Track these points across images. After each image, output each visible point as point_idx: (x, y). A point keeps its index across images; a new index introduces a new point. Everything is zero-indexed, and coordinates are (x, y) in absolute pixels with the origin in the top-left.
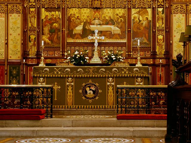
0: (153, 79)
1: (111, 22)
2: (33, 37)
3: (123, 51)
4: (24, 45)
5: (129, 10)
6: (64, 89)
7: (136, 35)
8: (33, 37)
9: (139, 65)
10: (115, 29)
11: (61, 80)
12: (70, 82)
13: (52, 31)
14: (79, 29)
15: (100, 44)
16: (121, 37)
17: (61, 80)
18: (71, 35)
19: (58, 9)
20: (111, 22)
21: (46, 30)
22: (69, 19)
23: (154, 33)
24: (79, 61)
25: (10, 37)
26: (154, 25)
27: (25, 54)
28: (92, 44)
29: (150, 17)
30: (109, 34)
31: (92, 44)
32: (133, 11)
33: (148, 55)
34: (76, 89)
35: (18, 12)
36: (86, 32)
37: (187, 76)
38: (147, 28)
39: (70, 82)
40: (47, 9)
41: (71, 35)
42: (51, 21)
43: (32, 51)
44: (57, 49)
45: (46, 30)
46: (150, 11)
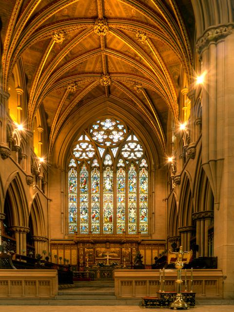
0: (18, 185)
1: (114, 252)
2: (82, 257)
3: (119, 262)
4: (78, 260)
5: (121, 249)
6: (96, 273)
7: (124, 256)
8: (82, 257)
9: (125, 266)
10: (115, 255)
11: (95, 271)
12: (98, 271)
13: (89, 255)
14: (101, 254)
15: (109, 259)
16: (118, 257)
17: (95, 271)
18: (97, 256)
19: (92, 248)
20: (114, 252)
21: (87, 255)
22: (97, 251)
23: (132, 256)
24: (101, 265)
25: (72, 257)
26: (132, 253)
27: (79, 263)
28: (106, 259)
29: (130, 251)
30: (113, 256)
31: (106, 259)
32: (123, 249)
33: (129, 263)
34: (101, 273)
35: (45, 240)
36: (103, 256)
37: (81, 262)
38: (129, 254)
39: (98, 271)
40: (87, 248)
41: (97, 256)
42: (89, 252)
43: (81, 262)
44: (92, 261)
45: (87, 255)
46: (130, 249)
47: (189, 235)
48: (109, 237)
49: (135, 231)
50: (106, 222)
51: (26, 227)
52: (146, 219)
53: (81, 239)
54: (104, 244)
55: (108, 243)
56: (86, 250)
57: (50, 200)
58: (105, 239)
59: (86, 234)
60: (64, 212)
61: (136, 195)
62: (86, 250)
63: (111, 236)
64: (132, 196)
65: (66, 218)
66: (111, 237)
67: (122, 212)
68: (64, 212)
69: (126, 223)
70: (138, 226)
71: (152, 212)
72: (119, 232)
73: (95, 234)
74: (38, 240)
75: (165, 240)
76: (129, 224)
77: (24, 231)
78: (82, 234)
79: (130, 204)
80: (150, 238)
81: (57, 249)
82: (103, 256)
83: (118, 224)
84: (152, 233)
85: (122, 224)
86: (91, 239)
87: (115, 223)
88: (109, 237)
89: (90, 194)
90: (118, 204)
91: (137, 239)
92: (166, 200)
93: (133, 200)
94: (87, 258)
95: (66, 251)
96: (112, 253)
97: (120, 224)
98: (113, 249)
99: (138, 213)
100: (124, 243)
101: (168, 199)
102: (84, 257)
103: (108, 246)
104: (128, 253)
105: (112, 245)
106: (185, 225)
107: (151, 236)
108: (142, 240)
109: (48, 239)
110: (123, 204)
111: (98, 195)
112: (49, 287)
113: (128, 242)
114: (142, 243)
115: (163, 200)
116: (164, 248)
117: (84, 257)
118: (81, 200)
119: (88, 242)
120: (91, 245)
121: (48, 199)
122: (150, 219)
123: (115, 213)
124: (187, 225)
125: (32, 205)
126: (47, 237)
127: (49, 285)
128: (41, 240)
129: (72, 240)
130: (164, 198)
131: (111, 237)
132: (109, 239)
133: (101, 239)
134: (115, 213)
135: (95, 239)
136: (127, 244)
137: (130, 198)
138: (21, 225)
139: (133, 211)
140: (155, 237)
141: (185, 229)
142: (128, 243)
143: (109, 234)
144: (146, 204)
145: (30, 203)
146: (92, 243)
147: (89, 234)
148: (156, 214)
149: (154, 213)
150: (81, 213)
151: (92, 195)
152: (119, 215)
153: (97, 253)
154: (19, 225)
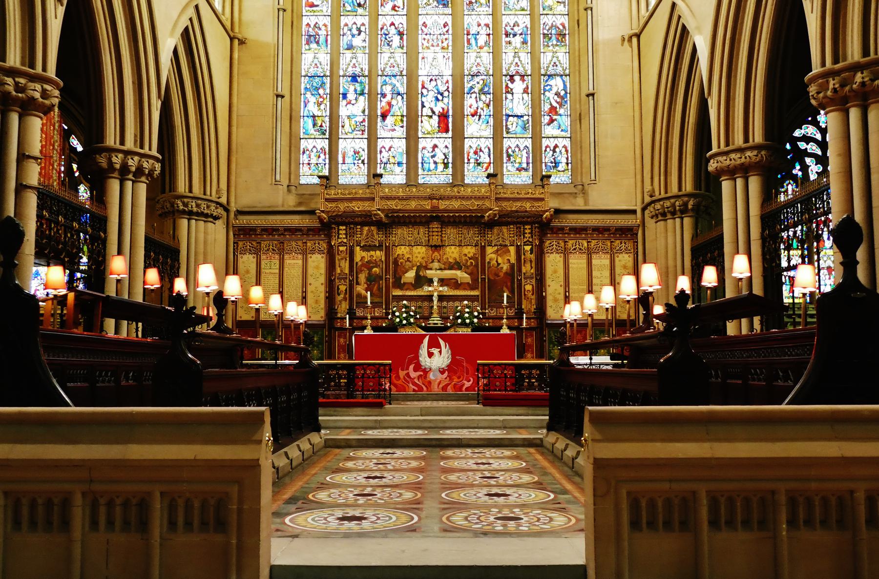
2: (343, 288)
5: (483, 249)
8: (343, 288)
10: (462, 275)
14: (410, 275)
15: (441, 298)
18: (399, 285)
19: (380, 247)
20: (456, 266)
21: (362, 277)
22: (396, 262)
28: (430, 298)
29: (513, 260)
32: (489, 250)
36: (421, 281)
40: (365, 248)
42: (369, 265)
45: (362, 277)
46: (512, 249)
47: (755, 183)
48: (441, 198)
49: (526, 170)
50: (429, 135)
51: (146, 150)
52: (564, 121)
53: (342, 207)
54: (422, 230)
55: (435, 225)
56: (359, 254)
57: (242, 42)
58: (427, 205)
59: (361, 186)
60: (286, 93)
61: (527, 19)
62: (359, 254)
63: (448, 192)
64: (516, 24)
65: (293, 118)
66: (449, 198)
67: (482, 92)
68: (286, 93)
69: (497, 137)
70: (537, 150)
71: (585, 92)
72: (475, 176)
73: (390, 186)
74: (190, 214)
75: (634, 212)
76: (506, 143)
77: (139, 171)
78: (345, 187)
79: (508, 58)
80: (579, 204)
81: (257, 252)
82: (421, 281)
83: (467, 143)
84: (586, 181)
85: (561, 143)
86: (374, 207)
87: (459, 139)
88: (441, 198)
89: (375, 17)
90: (470, 61)
91: (539, 206)
92: (635, 40)
93: (517, 41)
94: (360, 289)
95: (288, 262)
96: (451, 268)
97: (552, 143)
98: (452, 253)
99: (535, 95)
100: (491, 224)
101: (638, 36)
102: (351, 287)
103: (435, 240)
104: (505, 267)
105: (451, 232)
106: (738, 140)
107: (584, 192)
108: (558, 212)
109: (227, 210)
110: (486, 59)
111: (401, 21)
112: (219, 538)
113: (504, 220)
114: (556, 223)
115: (623, 40)
116: (630, 245)
117: (351, 287)
118: (344, 41)
119: (367, 219)
120: (378, 237)
121: (232, 39)
122: (578, 118)
123: (459, 94)
124: (746, 140)
125: (175, 52)
126: (223, 200)
127: (221, 525)
128: (202, 214)
129: (312, 212)
130: (627, 32)
131: (449, 198)
132: (443, 205)
133: (413, 205)
134: (459, 94)
135: (392, 205)
136: (505, 229)
137: (507, 35)
138: (130, 144)
139: (518, 86)
140: (600, 199)
141: (736, 159)
142: (507, 224)
143: (438, 186)
144: (563, 57)
145: (169, 42)
146: (380, 225)
147: (368, 186)
148: (602, 98)
149: (593, 95)
150: (345, 96)
151: (382, 20)
152: (470, 102)
153: (397, 267)
154: (122, 142)
